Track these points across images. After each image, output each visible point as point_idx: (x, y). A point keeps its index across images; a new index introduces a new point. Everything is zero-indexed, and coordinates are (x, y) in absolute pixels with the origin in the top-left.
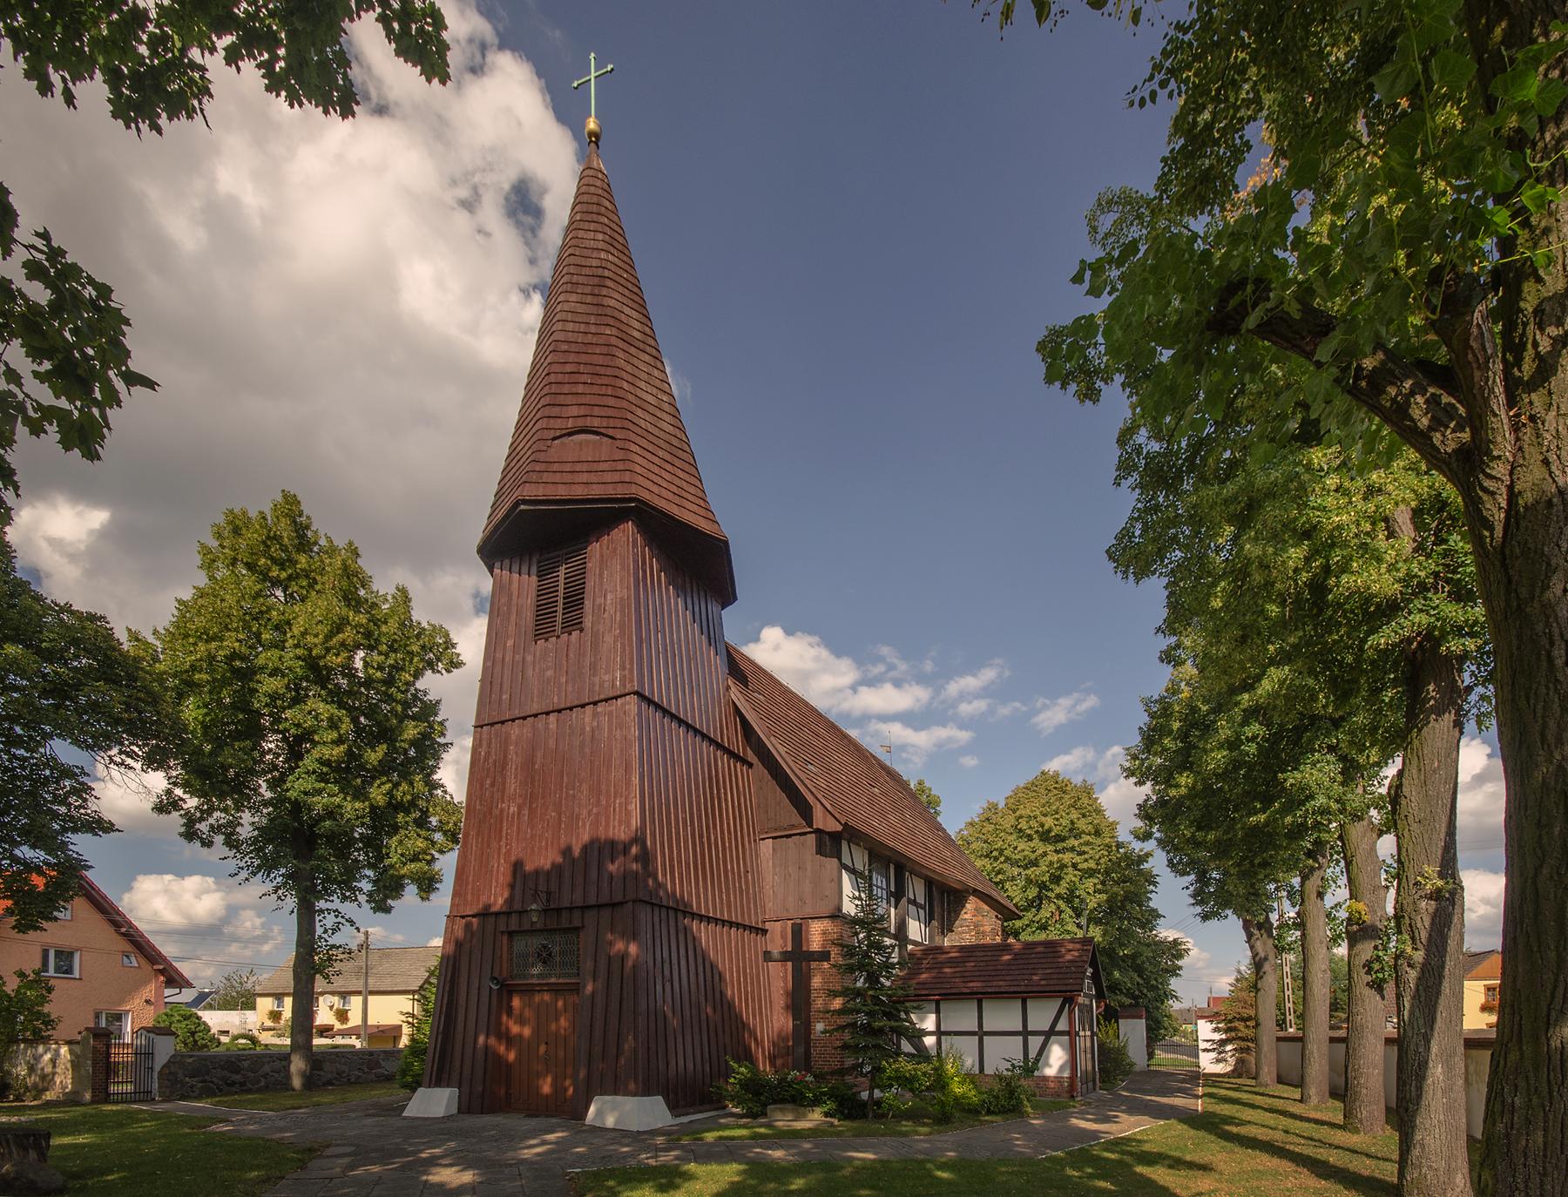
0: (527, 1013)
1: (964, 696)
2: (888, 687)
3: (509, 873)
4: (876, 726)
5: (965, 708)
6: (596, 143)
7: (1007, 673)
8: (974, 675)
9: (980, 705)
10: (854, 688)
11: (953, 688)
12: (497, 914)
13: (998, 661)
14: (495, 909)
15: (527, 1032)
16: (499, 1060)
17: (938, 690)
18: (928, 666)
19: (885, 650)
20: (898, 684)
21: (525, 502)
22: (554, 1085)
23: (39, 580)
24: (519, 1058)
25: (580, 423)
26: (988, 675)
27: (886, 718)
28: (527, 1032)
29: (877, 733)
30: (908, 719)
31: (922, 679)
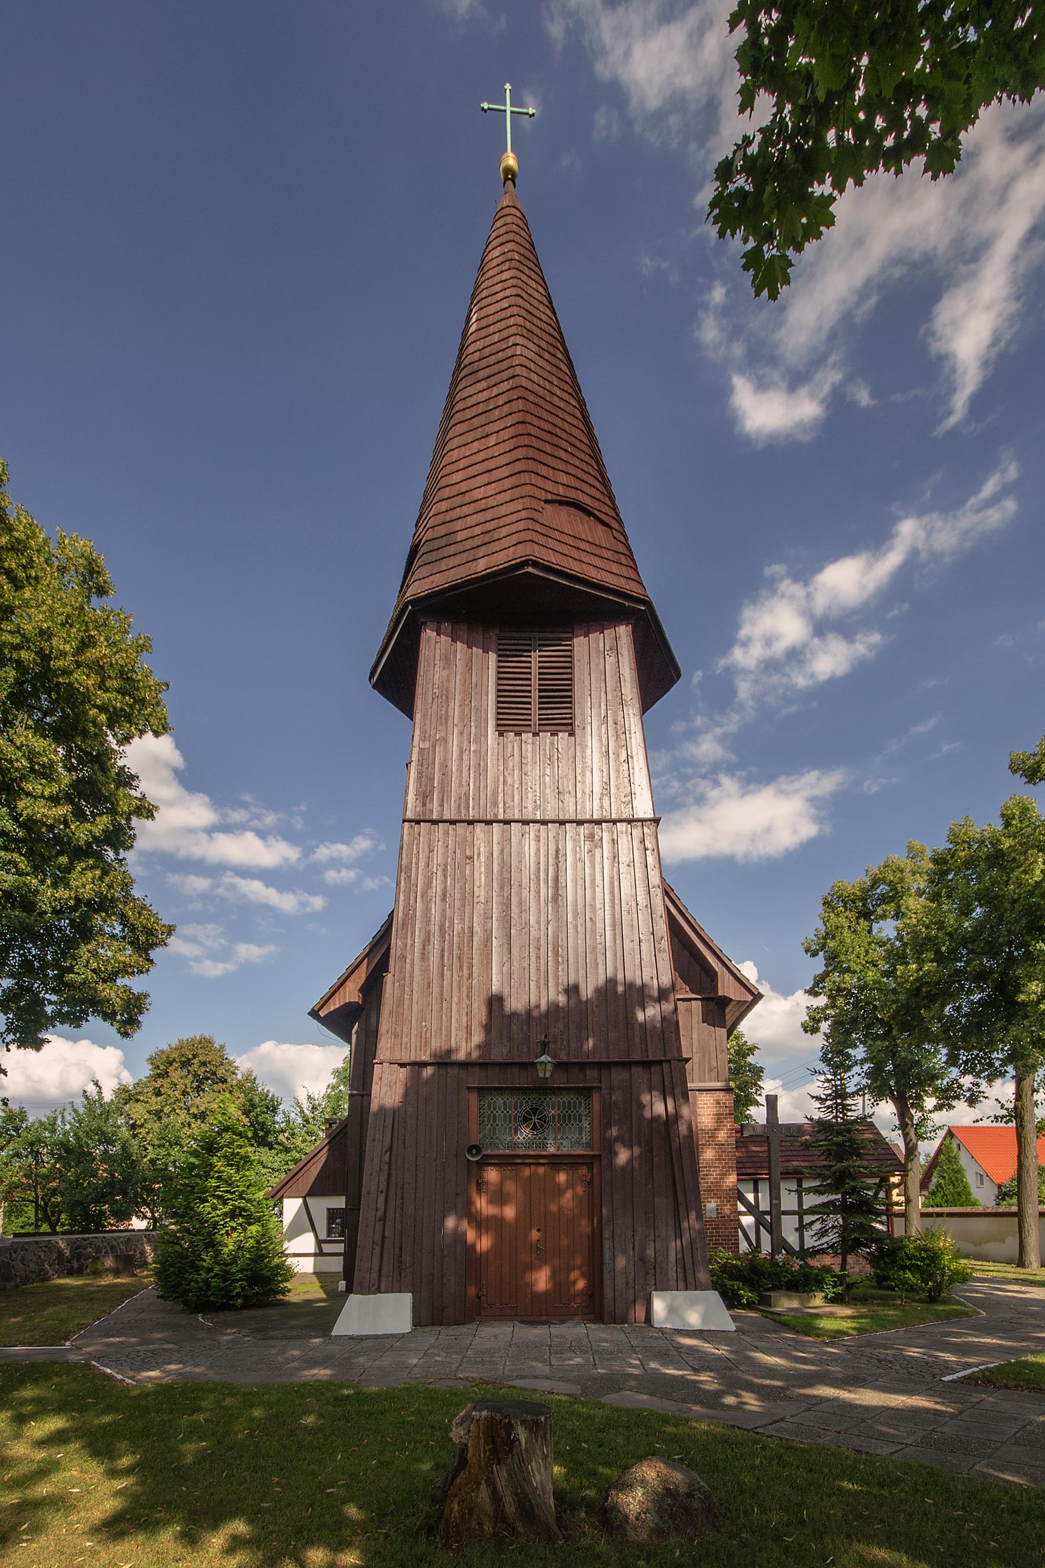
0: (510, 1187)
1: (334, 863)
2: (250, 836)
3: (484, 1008)
4: (229, 878)
5: (331, 876)
6: (513, 180)
7: (382, 847)
8: (347, 844)
9: (348, 875)
10: (210, 831)
11: (323, 853)
12: (462, 1065)
13: (368, 830)
14: (461, 1056)
15: (509, 1212)
16: (470, 1250)
17: (307, 852)
18: (299, 824)
19: (247, 798)
20: (262, 835)
21: (536, 564)
22: (553, 1277)
23: (874, 555)
24: (496, 1247)
25: (572, 494)
26: (363, 844)
27: (245, 872)
28: (509, 1212)
29: (232, 887)
30: (269, 876)
31: (289, 836)
